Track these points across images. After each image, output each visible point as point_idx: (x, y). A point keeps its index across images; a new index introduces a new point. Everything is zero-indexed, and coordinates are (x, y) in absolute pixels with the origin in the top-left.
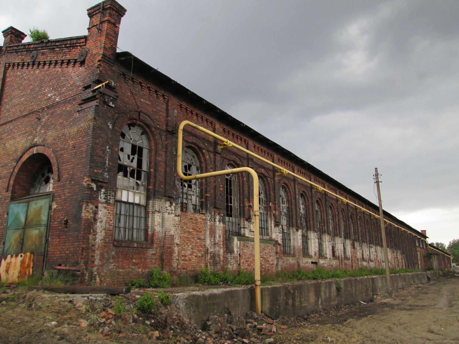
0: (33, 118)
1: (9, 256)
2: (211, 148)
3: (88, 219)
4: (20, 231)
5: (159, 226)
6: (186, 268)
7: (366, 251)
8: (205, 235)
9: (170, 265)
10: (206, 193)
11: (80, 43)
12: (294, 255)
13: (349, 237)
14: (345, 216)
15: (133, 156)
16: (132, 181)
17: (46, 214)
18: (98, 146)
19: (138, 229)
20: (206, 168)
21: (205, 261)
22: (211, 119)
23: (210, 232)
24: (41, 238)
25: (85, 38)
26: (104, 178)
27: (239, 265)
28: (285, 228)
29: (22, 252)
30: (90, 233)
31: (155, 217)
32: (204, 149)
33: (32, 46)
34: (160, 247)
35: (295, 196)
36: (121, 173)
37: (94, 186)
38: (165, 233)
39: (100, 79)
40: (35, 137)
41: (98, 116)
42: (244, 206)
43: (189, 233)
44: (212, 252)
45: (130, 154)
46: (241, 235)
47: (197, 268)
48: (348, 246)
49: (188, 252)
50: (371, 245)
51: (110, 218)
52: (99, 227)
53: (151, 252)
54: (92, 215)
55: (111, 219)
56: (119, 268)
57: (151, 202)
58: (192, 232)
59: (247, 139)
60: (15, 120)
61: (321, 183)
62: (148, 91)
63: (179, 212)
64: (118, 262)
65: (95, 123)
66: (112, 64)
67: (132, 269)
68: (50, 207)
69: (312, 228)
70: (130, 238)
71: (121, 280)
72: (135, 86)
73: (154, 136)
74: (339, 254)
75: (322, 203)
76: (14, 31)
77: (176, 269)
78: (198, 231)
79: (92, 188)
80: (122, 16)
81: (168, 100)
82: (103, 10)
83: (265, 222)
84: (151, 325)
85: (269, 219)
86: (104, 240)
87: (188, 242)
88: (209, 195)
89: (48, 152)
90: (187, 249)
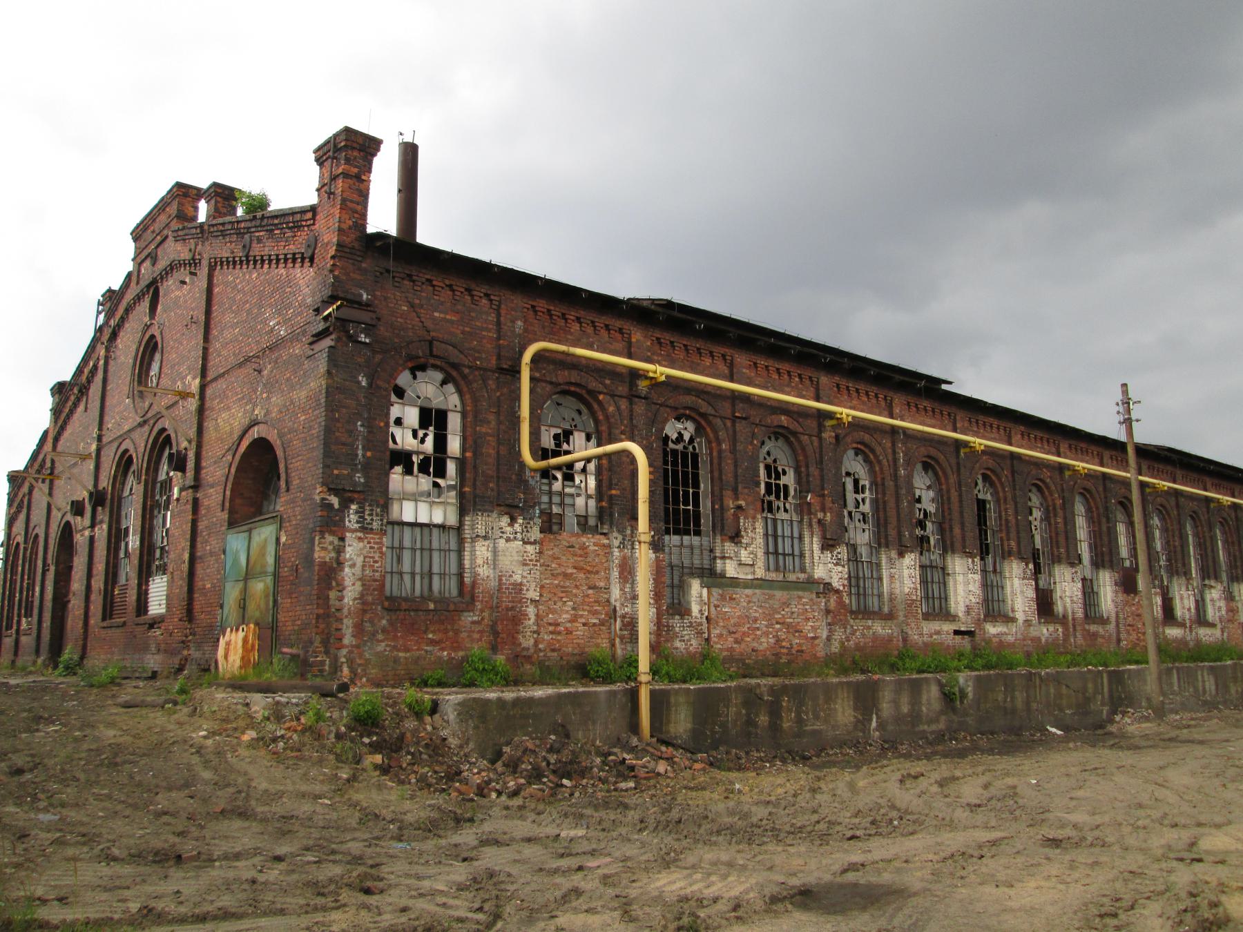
0: (249, 369)
1: (229, 629)
2: (620, 388)
3: (325, 562)
4: (241, 584)
5: (486, 566)
6: (560, 650)
7: (1182, 599)
8: (608, 579)
9: (514, 643)
10: (610, 488)
11: (306, 221)
12: (890, 616)
13: (1107, 564)
14: (1097, 508)
15: (424, 431)
16: (425, 482)
17: (273, 553)
18: (338, 425)
19: (442, 575)
20: (610, 434)
21: (610, 633)
22: (618, 323)
23: (621, 573)
24: (267, 596)
25: (313, 209)
26: (355, 484)
27: (707, 640)
28: (864, 551)
29: (243, 623)
30: (330, 588)
31: (477, 548)
32: (600, 393)
33: (243, 225)
34: (491, 608)
35: (896, 470)
36: (398, 469)
37: (335, 501)
38: (500, 580)
39: (335, 294)
40: (255, 406)
41: (335, 366)
42: (723, 509)
43: (566, 576)
44: (626, 614)
45: (417, 426)
46: (716, 574)
47: (587, 649)
48: (1105, 586)
49: (564, 616)
50: (1207, 582)
51: (373, 557)
52: (349, 575)
53: (469, 618)
54: (333, 555)
55: (377, 559)
56: (399, 650)
57: (467, 518)
58: (572, 574)
59: (729, 351)
60: (227, 372)
61: (998, 428)
62: (450, 293)
63: (535, 534)
64: (395, 638)
65: (330, 381)
66: (360, 259)
67: (426, 651)
68: (278, 540)
69: (958, 545)
70: (426, 593)
71: (403, 672)
72: (419, 288)
73: (468, 383)
74: (1065, 607)
75: (1000, 480)
76: (219, 191)
77: (532, 651)
78: (589, 572)
79: (331, 506)
80: (374, 155)
81: (500, 302)
82: (334, 152)
83: (796, 541)
84: (370, 745)
85: (806, 534)
86: (360, 599)
87: (563, 595)
88: (618, 492)
89: (273, 437)
90: (562, 610)
